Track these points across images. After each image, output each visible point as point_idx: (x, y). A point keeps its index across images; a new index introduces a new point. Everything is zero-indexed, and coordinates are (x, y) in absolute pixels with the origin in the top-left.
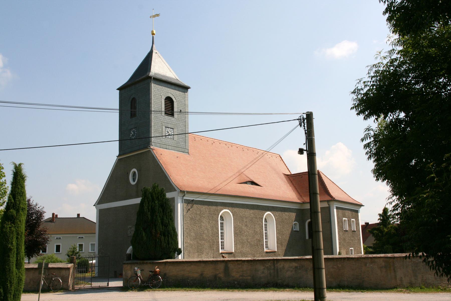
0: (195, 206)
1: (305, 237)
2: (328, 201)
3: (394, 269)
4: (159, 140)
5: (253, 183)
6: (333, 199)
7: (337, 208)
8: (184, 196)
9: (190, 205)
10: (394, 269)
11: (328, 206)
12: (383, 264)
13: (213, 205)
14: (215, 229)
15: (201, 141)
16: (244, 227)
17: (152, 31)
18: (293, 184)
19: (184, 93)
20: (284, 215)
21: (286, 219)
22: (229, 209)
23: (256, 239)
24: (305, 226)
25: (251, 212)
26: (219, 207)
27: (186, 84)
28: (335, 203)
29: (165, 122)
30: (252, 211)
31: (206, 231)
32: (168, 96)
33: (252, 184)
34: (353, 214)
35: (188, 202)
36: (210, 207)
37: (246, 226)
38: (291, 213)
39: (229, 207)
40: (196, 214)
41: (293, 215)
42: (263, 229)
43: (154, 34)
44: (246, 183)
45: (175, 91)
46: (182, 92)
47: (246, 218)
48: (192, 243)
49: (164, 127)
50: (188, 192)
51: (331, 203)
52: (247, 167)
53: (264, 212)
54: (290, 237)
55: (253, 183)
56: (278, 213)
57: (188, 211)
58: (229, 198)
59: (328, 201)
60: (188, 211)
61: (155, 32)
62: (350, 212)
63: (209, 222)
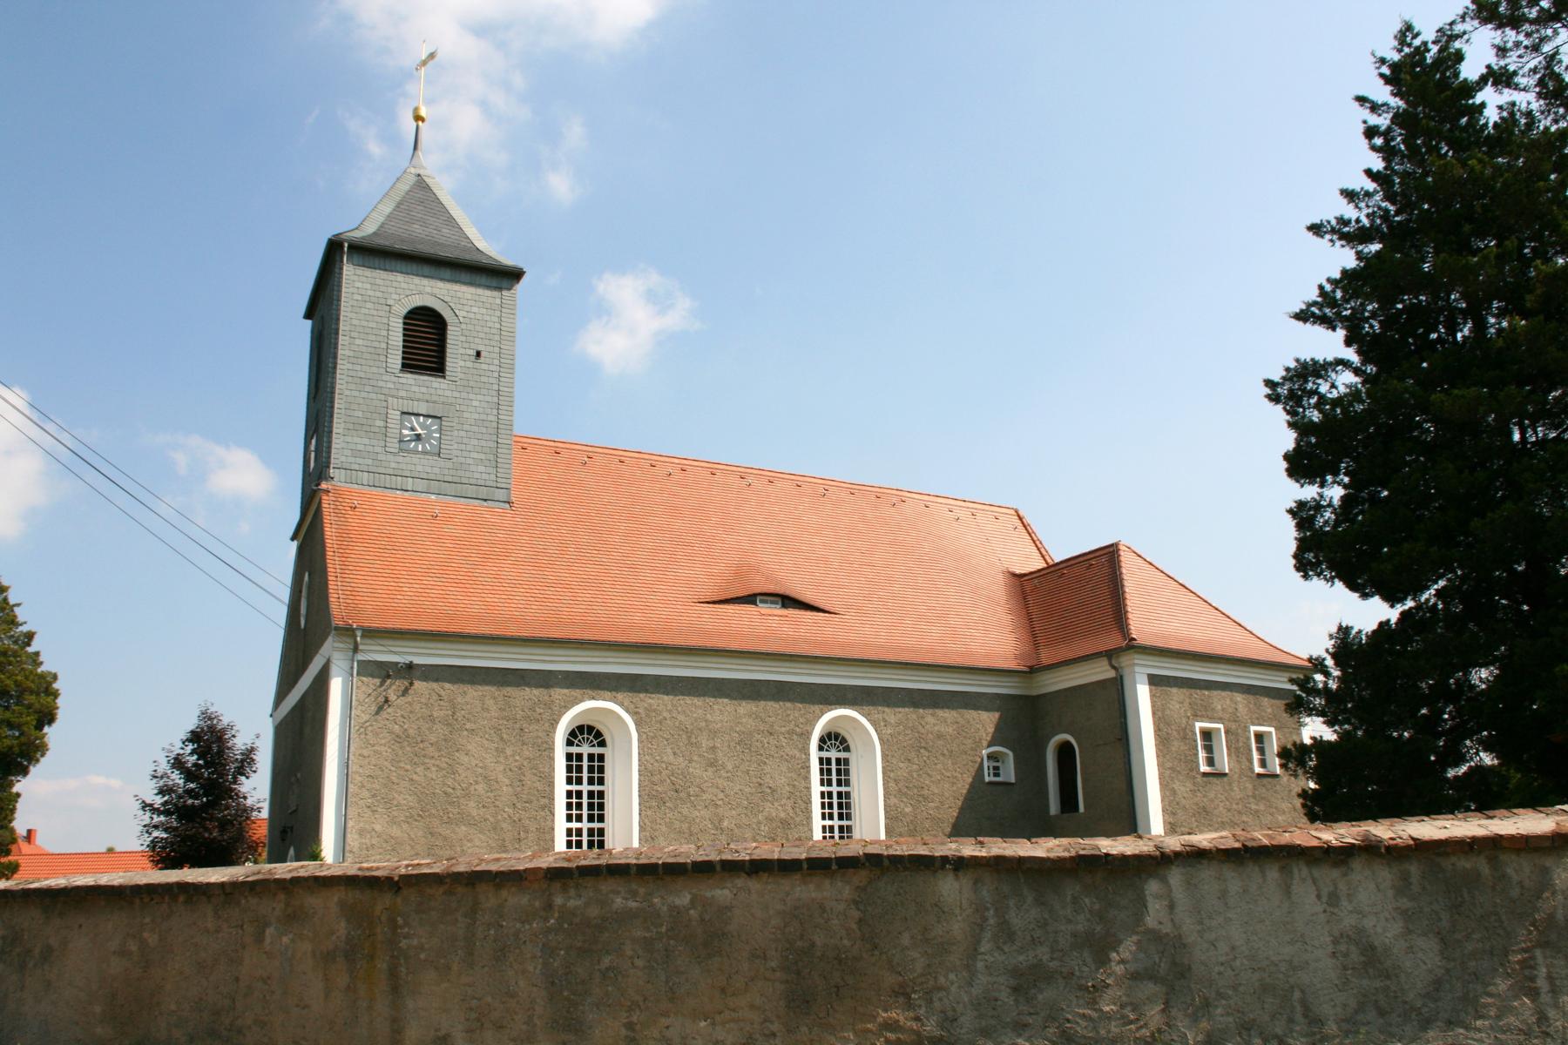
0: (419, 685)
1: (1047, 806)
2: (1110, 655)
3: (393, 974)
4: (370, 462)
5: (789, 601)
6: (1132, 646)
7: (1154, 681)
8: (356, 650)
9: (393, 689)
10: (393, 974)
11: (1111, 674)
12: (342, 928)
13: (528, 685)
14: (529, 779)
15: (620, 465)
16: (696, 770)
17: (416, 110)
18: (1026, 607)
19: (496, 294)
20: (930, 719)
21: (940, 736)
22: (621, 705)
23: (770, 819)
24: (1045, 767)
25: (741, 710)
26: (559, 693)
27: (508, 260)
28: (1139, 659)
29: (403, 394)
30: (745, 707)
31: (481, 788)
32: (409, 308)
33: (784, 606)
34: (1259, 707)
35: (384, 672)
36: (509, 690)
37: (712, 764)
38: (971, 714)
39: (616, 689)
40: (431, 718)
41: (986, 722)
42: (807, 778)
43: (423, 120)
44: (750, 599)
45: (457, 287)
46: (488, 287)
47: (714, 734)
48: (395, 831)
49: (395, 415)
50: (370, 633)
51: (1125, 660)
52: (410, 484)
53: (817, 708)
54: (962, 810)
55: (789, 601)
56: (892, 715)
57: (380, 709)
58: (611, 656)
59: (1110, 655)
60: (380, 709)
61: (423, 113)
62: (1239, 697)
63: (500, 751)
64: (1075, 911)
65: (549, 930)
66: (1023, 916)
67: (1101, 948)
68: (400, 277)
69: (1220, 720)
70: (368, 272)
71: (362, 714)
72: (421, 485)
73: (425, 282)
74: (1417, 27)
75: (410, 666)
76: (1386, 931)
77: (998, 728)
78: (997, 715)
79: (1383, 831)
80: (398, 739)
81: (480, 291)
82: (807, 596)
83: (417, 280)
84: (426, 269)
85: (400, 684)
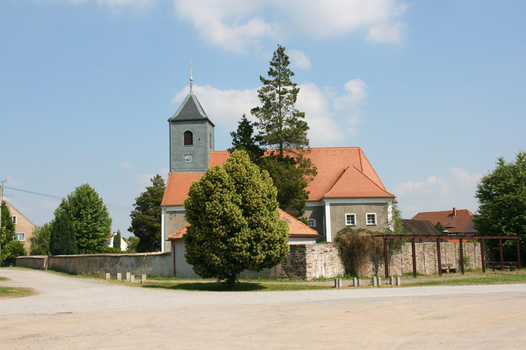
0: (177, 214)
7: (331, 205)
35: (171, 213)
64: (116, 260)
65: (520, 243)
66: (113, 260)
67: (117, 263)
68: (182, 125)
69: (355, 212)
70: (176, 126)
71: (167, 221)
72: (189, 170)
73: (187, 125)
74: (293, 76)
75: (176, 211)
76: (134, 262)
77: (312, 215)
78: (312, 211)
79: (154, 253)
80: (174, 225)
81: (199, 125)
82: (339, 171)
83: (186, 125)
84: (188, 122)
85: (174, 215)
